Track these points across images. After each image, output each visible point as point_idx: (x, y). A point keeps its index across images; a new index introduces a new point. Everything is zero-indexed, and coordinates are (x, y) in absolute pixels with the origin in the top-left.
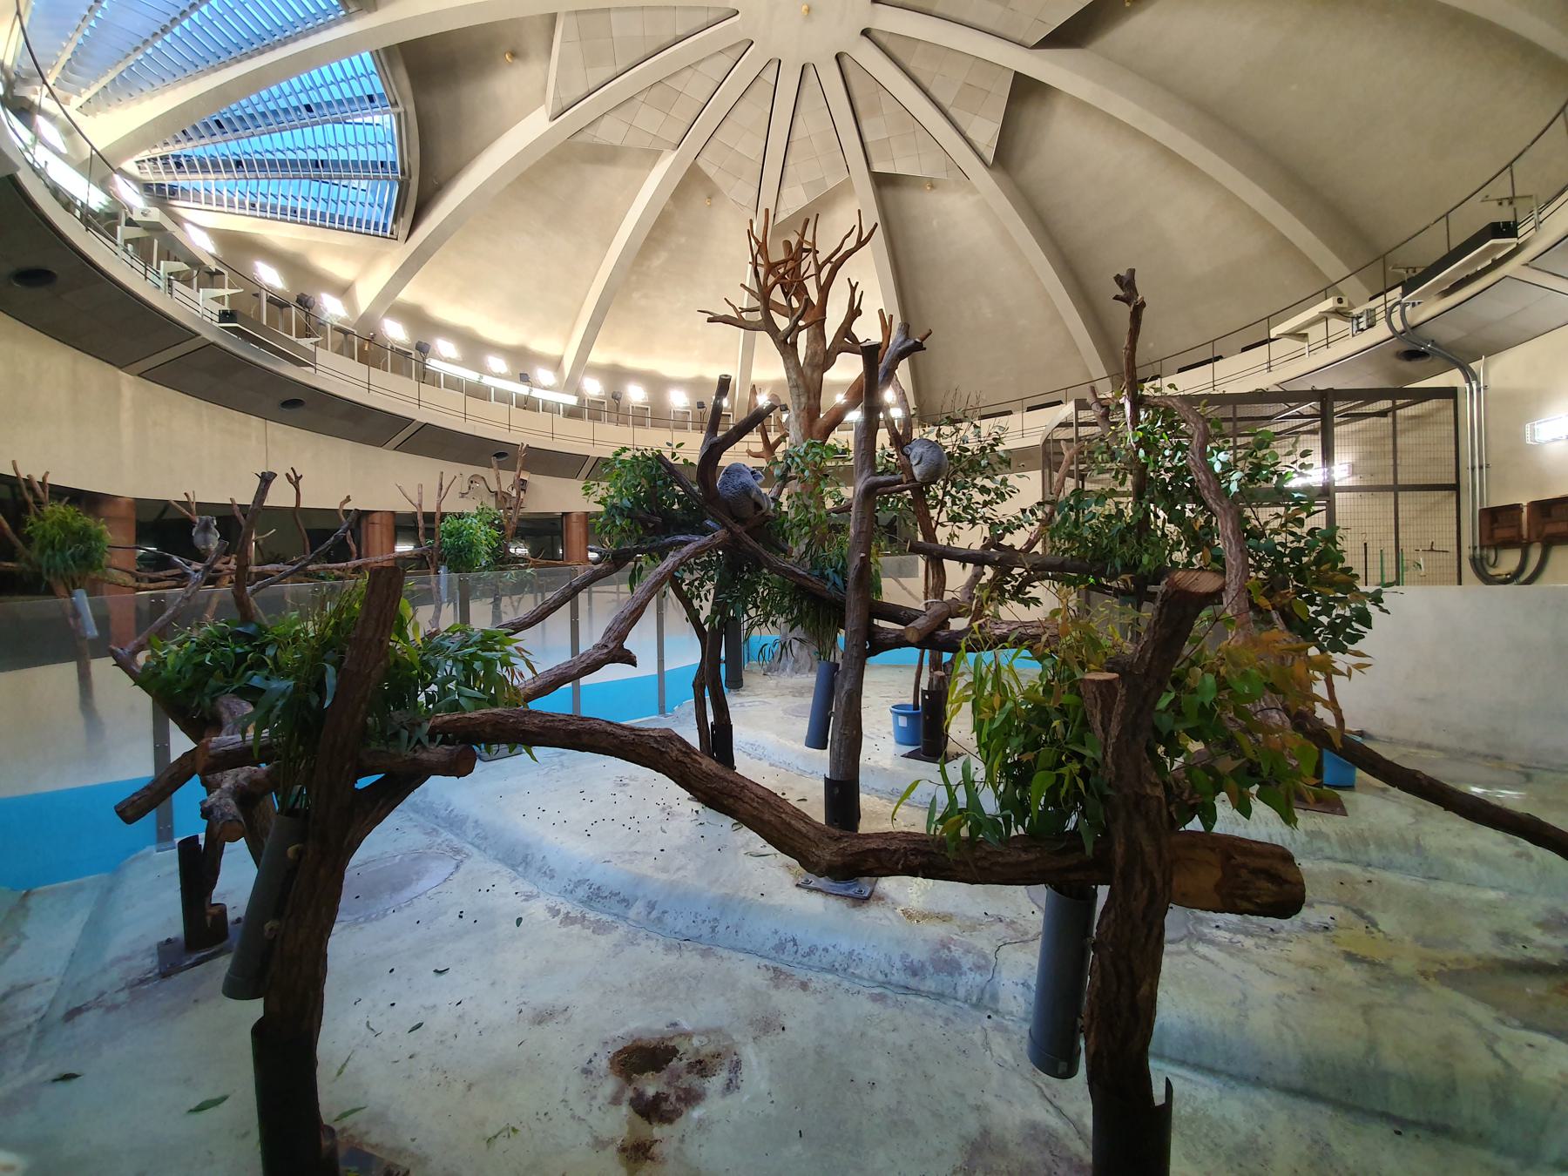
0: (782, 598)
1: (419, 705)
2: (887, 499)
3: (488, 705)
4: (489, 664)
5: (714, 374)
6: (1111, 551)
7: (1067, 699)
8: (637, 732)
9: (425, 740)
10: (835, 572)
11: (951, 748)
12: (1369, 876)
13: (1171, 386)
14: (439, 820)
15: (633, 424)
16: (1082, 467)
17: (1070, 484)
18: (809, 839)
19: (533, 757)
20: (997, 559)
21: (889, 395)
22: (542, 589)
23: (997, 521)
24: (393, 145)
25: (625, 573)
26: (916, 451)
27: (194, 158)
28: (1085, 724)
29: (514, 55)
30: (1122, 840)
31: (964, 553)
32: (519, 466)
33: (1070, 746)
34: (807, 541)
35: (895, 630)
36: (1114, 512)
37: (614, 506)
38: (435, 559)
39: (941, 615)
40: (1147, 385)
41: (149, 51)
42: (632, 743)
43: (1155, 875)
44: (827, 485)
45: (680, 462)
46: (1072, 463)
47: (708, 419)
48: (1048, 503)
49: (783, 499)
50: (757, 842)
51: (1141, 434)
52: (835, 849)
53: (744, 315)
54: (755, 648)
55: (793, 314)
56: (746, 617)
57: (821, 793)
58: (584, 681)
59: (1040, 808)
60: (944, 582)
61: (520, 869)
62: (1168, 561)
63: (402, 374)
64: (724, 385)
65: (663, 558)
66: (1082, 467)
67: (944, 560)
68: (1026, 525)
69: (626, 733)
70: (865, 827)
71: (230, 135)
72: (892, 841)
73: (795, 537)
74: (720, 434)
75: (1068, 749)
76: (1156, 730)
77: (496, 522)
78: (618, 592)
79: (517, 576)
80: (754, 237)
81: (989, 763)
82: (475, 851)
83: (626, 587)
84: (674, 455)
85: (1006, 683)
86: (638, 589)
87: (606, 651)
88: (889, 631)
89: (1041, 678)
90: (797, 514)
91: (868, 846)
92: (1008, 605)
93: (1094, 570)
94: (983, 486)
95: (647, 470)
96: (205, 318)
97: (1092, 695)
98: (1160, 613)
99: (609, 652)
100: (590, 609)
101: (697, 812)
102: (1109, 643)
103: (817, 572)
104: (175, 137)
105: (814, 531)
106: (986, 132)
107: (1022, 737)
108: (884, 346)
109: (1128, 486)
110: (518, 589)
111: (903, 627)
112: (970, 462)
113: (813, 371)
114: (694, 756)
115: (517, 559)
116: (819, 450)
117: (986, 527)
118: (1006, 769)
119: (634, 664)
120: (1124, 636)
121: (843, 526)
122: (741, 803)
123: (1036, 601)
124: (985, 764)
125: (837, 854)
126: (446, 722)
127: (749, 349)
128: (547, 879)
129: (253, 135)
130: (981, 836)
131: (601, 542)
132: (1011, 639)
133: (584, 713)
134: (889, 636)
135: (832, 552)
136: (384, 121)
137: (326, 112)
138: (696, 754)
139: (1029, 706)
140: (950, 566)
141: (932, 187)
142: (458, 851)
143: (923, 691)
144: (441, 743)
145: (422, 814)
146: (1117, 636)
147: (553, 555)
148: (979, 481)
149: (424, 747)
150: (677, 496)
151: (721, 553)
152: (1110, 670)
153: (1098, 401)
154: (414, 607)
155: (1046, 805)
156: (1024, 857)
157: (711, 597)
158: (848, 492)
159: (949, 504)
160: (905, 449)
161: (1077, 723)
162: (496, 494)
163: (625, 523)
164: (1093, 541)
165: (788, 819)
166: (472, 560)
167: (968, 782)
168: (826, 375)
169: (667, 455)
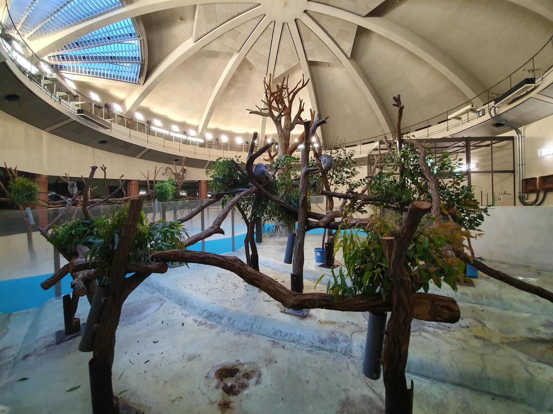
0: (276, 211)
1: (148, 248)
2: (313, 176)
3: (172, 248)
4: (172, 234)
5: (252, 132)
6: (392, 194)
7: (376, 246)
8: (224, 258)
9: (150, 260)
10: (295, 201)
11: (335, 263)
12: (483, 308)
13: (413, 136)
14: (155, 289)
15: (223, 149)
16: (382, 164)
17: (378, 170)
18: (285, 295)
19: (188, 267)
20: (352, 197)
21: (313, 139)
22: (191, 207)
23: (352, 183)
24: (139, 51)
25: (220, 202)
26: (323, 159)
27: (68, 56)
28: (383, 255)
29: (181, 19)
30: (396, 296)
31: (340, 195)
32: (183, 164)
33: (377, 263)
34: (285, 190)
35: (316, 222)
36: (393, 180)
37: (217, 178)
38: (153, 197)
39: (332, 216)
40: (404, 136)
41: (53, 18)
42: (223, 262)
43: (408, 308)
44: (292, 171)
45: (240, 163)
46: (378, 163)
47: (250, 147)
48: (369, 177)
49: (276, 176)
50: (267, 297)
51: (402, 153)
52: (295, 299)
53: (262, 111)
54: (266, 228)
55: (280, 111)
56: (263, 217)
57: (290, 279)
58: (206, 240)
59: (367, 285)
60: (333, 205)
61: (183, 306)
62: (412, 197)
63: (142, 132)
64: (255, 136)
65: (234, 197)
66: (382, 164)
67: (333, 197)
68: (362, 185)
69: (221, 258)
70: (305, 291)
71: (81, 47)
72: (315, 296)
73: (280, 189)
74: (254, 153)
75: (377, 264)
76: (408, 257)
77: (175, 184)
78: (218, 209)
79: (182, 203)
80: (266, 83)
81: (349, 269)
82: (168, 299)
83: (221, 207)
84: (238, 160)
85: (355, 240)
86: (225, 208)
87: (214, 229)
88: (313, 222)
89: (367, 239)
90: (281, 181)
91: (306, 298)
92: (356, 213)
93: (386, 201)
94: (347, 171)
95: (228, 165)
96: (72, 112)
97: (385, 245)
98: (409, 216)
99: (215, 230)
100: (208, 215)
101: (246, 286)
102: (391, 226)
103: (288, 202)
104: (62, 48)
105: (287, 187)
106: (348, 47)
107: (360, 259)
108: (312, 122)
109: (398, 171)
110: (183, 207)
111: (318, 221)
112: (342, 163)
113: (287, 131)
114: (245, 266)
115: (182, 197)
116: (289, 159)
117: (348, 186)
118: (355, 271)
119: (224, 234)
120: (396, 224)
121: (297, 185)
122: (261, 283)
123: (365, 212)
124: (348, 269)
125: (295, 301)
126: (157, 254)
127: (264, 123)
128: (193, 309)
129: (89, 48)
130: (346, 294)
131: (212, 191)
132: (356, 225)
133: (206, 251)
134: (314, 224)
135: (294, 194)
136: (136, 43)
137: (115, 39)
138: (245, 265)
139: (363, 249)
140: (335, 199)
141: (329, 66)
142: (161, 300)
143: (325, 243)
144: (155, 262)
145: (149, 287)
146: (394, 224)
147: (195, 196)
148: (345, 169)
149: (150, 263)
150: (239, 175)
151: (254, 195)
152: (391, 236)
153: (387, 141)
154: (146, 214)
155: (369, 284)
156: (361, 302)
157: (251, 210)
158: (299, 173)
159: (335, 177)
160: (319, 158)
161: (380, 254)
162: (175, 174)
163: (220, 184)
164: (385, 191)
165: (278, 288)
166: (166, 197)
167: (341, 275)
168: (291, 132)
169: (235, 160)
